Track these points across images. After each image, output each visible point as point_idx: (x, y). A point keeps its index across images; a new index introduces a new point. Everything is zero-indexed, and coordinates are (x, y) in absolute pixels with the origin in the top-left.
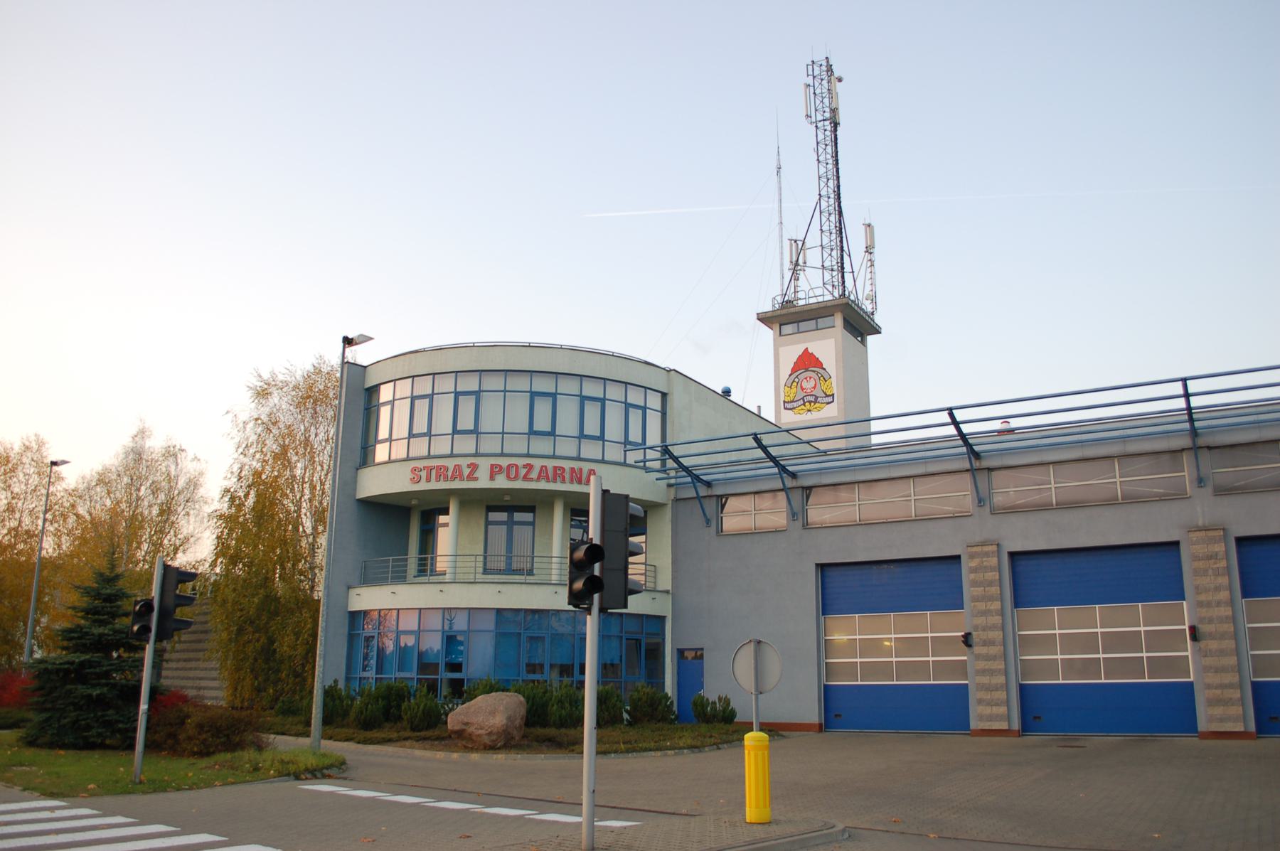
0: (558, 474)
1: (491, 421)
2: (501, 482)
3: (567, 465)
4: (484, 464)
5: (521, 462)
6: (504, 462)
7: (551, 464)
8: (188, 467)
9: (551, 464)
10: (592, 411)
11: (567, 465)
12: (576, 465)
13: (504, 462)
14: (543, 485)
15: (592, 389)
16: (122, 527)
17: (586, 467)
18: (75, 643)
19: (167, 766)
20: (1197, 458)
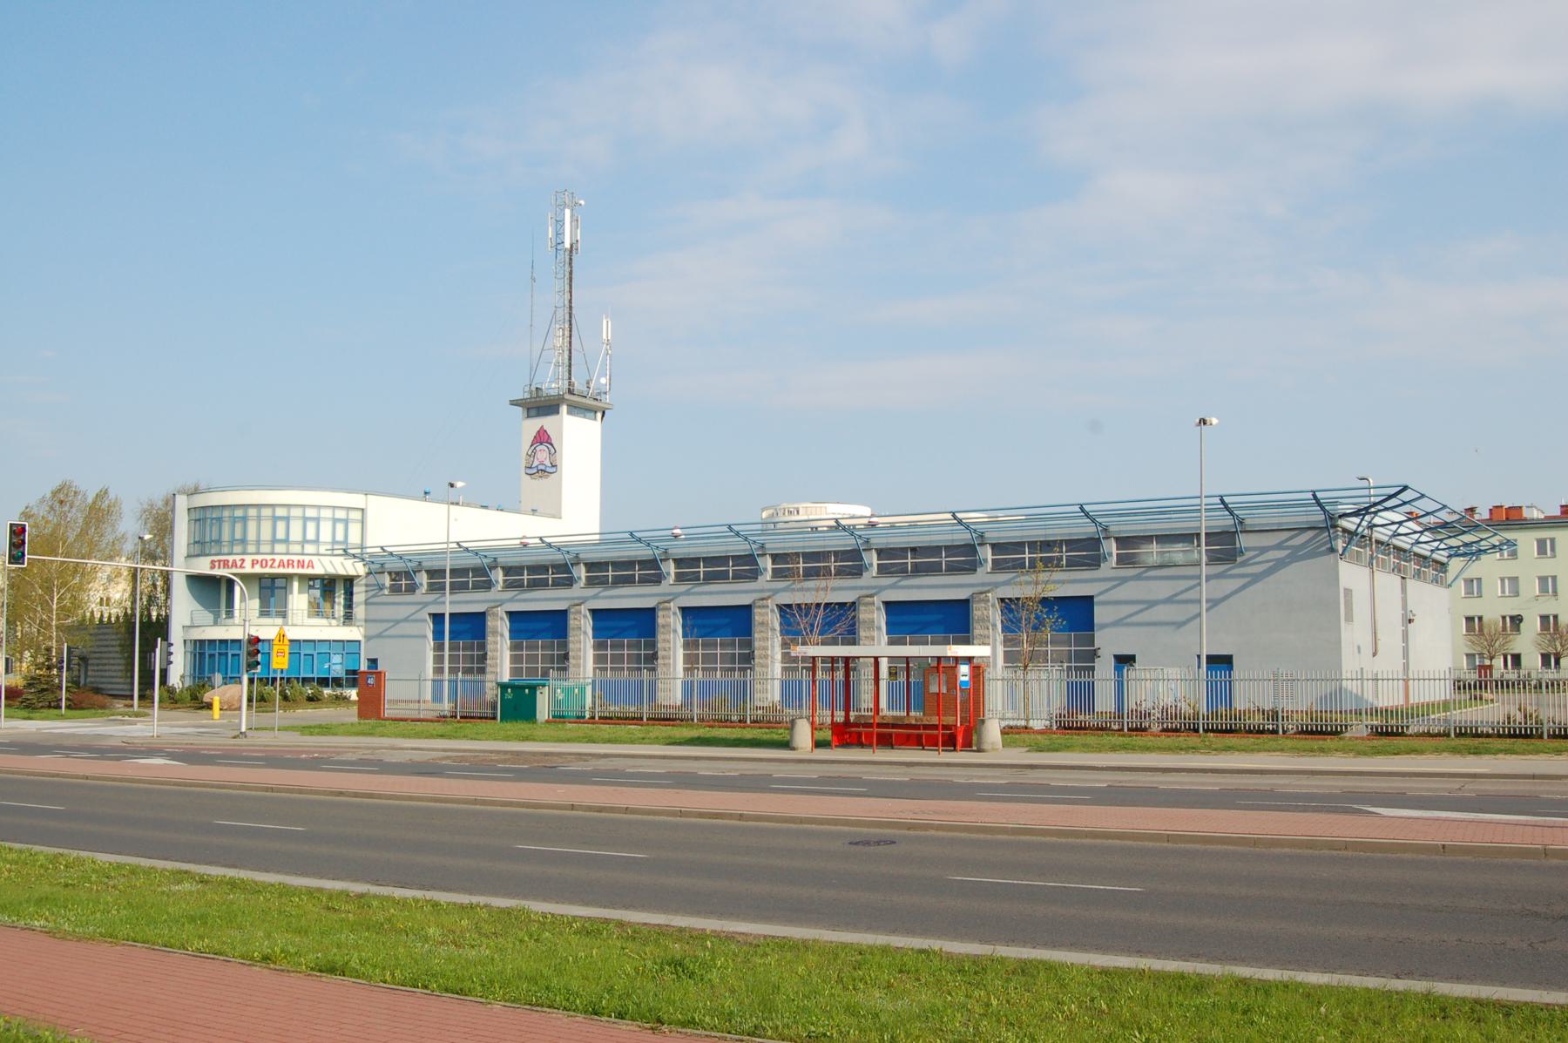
0: (290, 563)
1: (266, 527)
2: (258, 569)
3: (295, 558)
4: (248, 559)
5: (269, 557)
6: (259, 558)
7: (285, 558)
8: (1187, 709)
9: (285, 558)
10: (311, 526)
11: (295, 558)
12: (301, 558)
13: (259, 558)
14: (282, 571)
15: (310, 513)
16: (77, 516)
17: (307, 559)
18: (23, 670)
19: (71, 713)
20: (1404, 589)
